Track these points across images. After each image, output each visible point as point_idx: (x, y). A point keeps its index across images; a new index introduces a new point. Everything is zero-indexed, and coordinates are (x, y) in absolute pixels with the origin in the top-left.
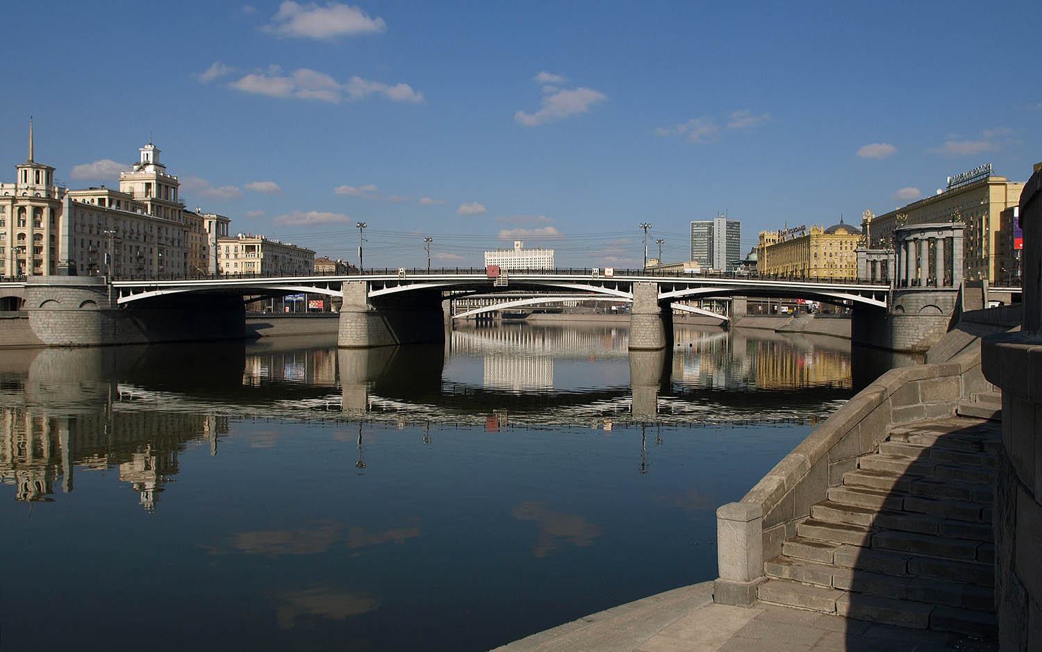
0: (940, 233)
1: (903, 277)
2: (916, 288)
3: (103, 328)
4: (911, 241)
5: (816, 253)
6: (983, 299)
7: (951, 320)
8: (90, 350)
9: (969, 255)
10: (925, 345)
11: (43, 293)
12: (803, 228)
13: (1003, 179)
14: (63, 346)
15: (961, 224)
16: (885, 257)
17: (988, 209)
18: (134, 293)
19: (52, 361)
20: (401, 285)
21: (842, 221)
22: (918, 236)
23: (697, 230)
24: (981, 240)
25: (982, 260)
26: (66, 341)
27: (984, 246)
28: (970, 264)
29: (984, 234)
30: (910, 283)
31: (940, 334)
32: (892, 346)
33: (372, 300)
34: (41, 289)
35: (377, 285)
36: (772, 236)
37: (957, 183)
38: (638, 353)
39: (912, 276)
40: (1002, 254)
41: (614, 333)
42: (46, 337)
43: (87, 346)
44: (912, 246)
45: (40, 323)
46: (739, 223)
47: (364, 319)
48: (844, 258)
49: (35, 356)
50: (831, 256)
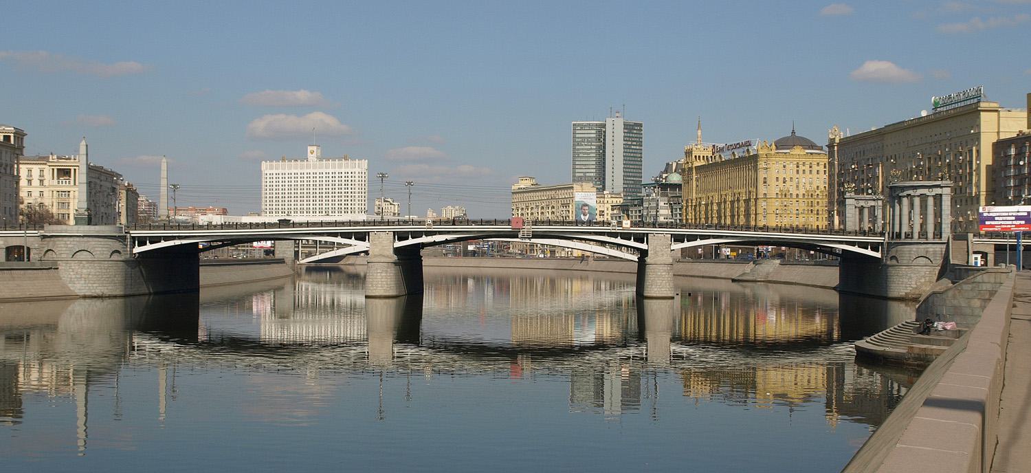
0: (931, 190)
1: (897, 230)
2: (909, 241)
3: (128, 280)
4: (904, 197)
5: (765, 178)
6: (968, 252)
7: (940, 270)
8: (118, 301)
9: (958, 191)
10: (917, 293)
11: (75, 243)
12: (748, 144)
13: (995, 105)
14: (95, 297)
15: (949, 182)
16: (873, 203)
17: (978, 139)
18: (151, 243)
19: (85, 312)
20: (426, 236)
21: (793, 132)
22: (911, 192)
23: (581, 134)
24: (971, 174)
25: (972, 198)
26: (98, 292)
27: (974, 182)
28: (958, 201)
29: (974, 168)
30: (903, 236)
31: (930, 282)
32: (887, 293)
33: (397, 251)
34: (71, 239)
35: (402, 236)
36: (703, 151)
37: (945, 105)
38: (655, 301)
39: (905, 229)
40: (994, 191)
41: (470, 282)
42: (79, 288)
43: (115, 297)
44: (905, 201)
45: (71, 273)
46: (641, 125)
47: (393, 269)
48: (801, 186)
49: (70, 304)
50: (784, 182)
